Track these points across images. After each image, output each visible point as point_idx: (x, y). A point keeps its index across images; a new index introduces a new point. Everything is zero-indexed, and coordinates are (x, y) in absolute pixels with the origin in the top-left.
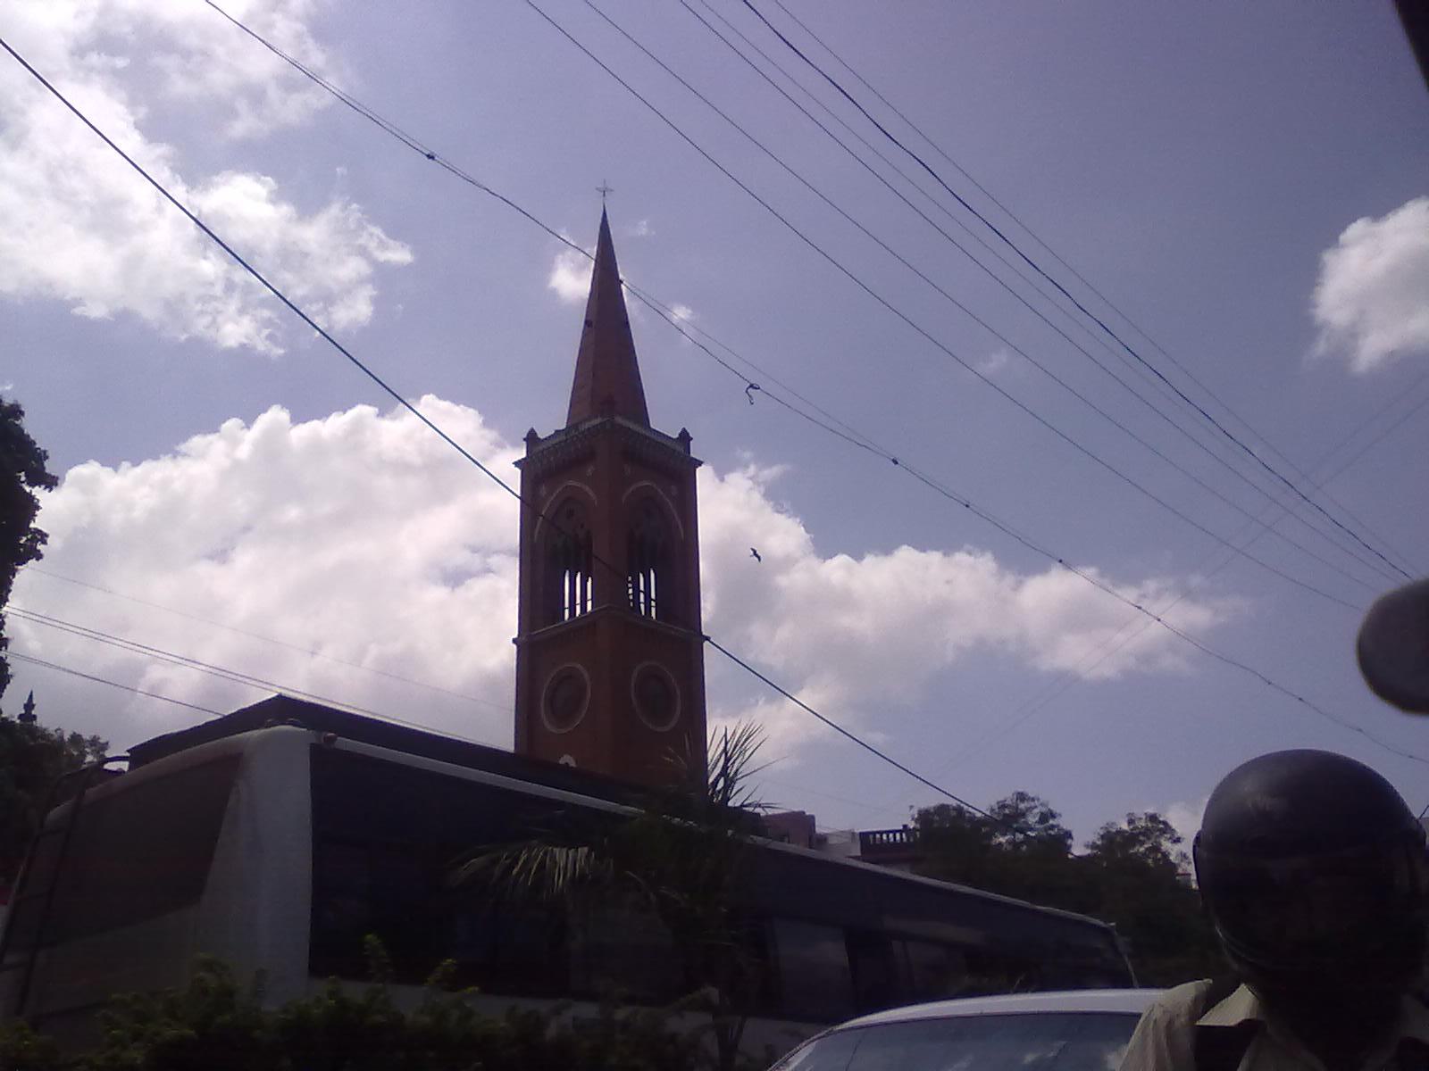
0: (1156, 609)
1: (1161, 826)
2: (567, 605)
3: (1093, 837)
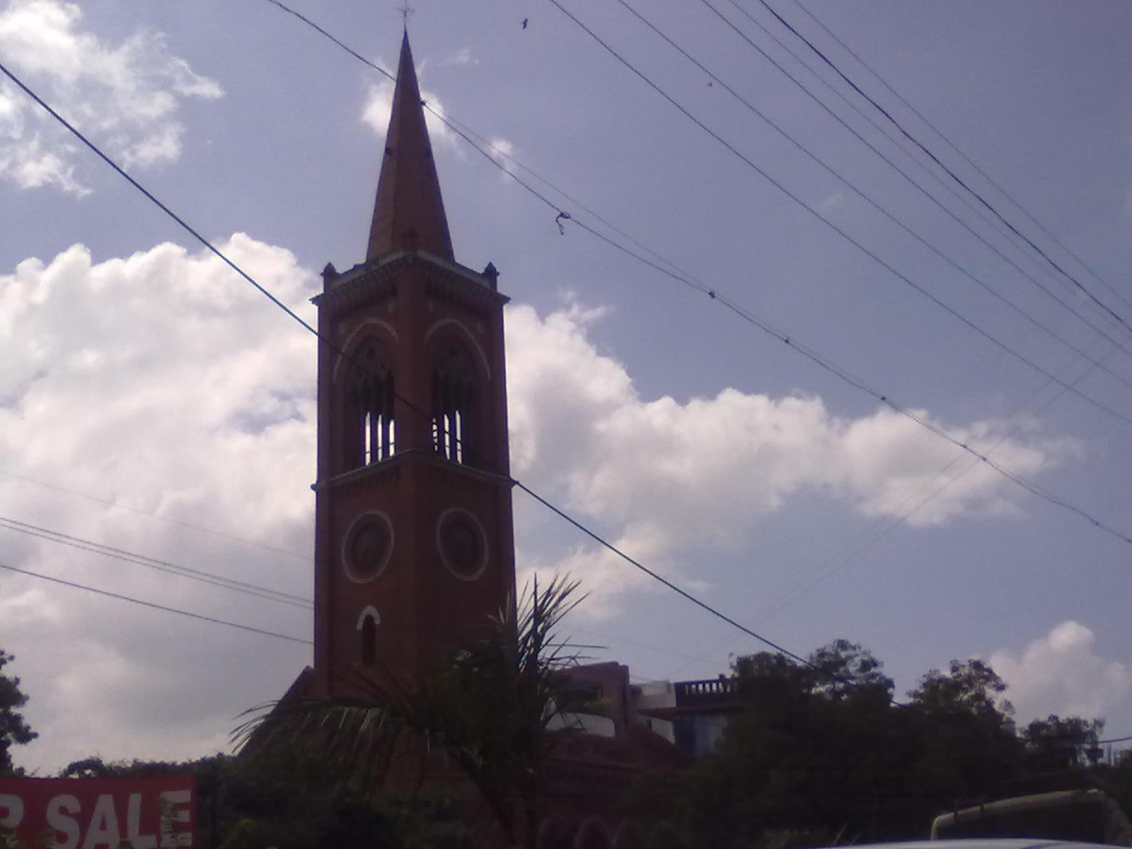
0: (981, 449)
1: (986, 673)
2: (368, 448)
3: (916, 686)
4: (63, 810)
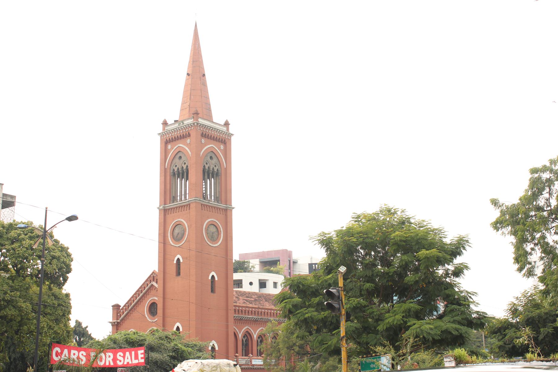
4: (120, 355)
